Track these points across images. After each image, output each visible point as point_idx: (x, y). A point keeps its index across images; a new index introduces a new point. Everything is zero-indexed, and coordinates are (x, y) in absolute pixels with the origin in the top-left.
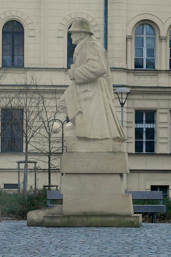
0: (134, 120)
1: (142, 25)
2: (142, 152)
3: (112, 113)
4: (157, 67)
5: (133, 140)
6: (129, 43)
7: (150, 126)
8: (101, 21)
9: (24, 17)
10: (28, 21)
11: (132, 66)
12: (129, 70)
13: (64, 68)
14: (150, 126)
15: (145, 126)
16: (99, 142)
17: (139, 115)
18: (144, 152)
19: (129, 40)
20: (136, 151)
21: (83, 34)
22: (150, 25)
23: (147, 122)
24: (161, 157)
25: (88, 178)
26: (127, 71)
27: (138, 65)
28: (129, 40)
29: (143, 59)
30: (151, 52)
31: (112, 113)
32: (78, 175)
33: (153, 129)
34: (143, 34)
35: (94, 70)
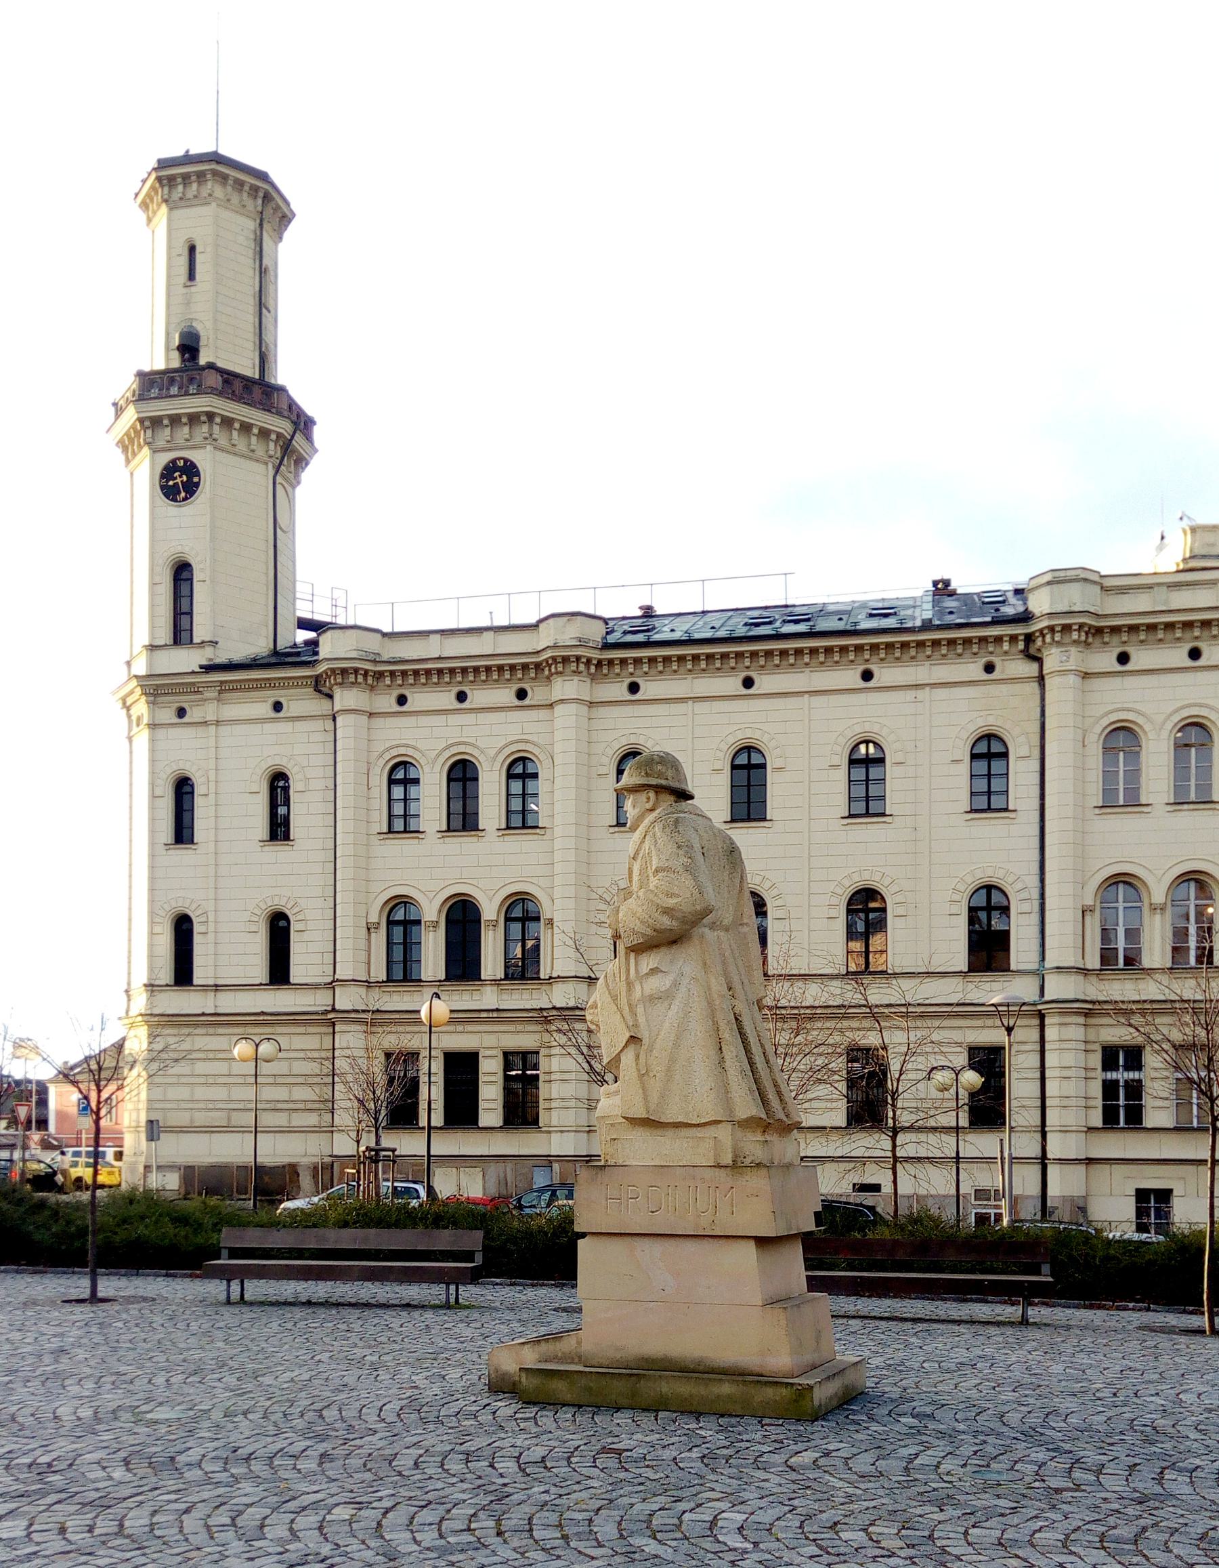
0: (1099, 1066)
1: (1114, 883)
2: (1119, 1124)
3: (742, 1033)
4: (1146, 962)
5: (1099, 1103)
6: (1088, 918)
7: (1132, 1075)
8: (1034, 881)
9: (877, 877)
10: (886, 881)
11: (1094, 962)
12: (1088, 970)
13: (961, 972)
14: (1132, 1075)
15: (1122, 1076)
16: (685, 1132)
17: (1110, 1057)
18: (1122, 1124)
19: (1088, 912)
20: (1104, 1123)
21: (652, 794)
22: (1125, 882)
23: (1127, 1068)
24: (1156, 1135)
25: (657, 1247)
26: (1084, 972)
27: (1107, 957)
28: (1088, 912)
29: (1117, 949)
30: (1133, 934)
31: (742, 1033)
32: (629, 1239)
33: (1140, 1081)
34: (1117, 902)
35: (671, 902)
